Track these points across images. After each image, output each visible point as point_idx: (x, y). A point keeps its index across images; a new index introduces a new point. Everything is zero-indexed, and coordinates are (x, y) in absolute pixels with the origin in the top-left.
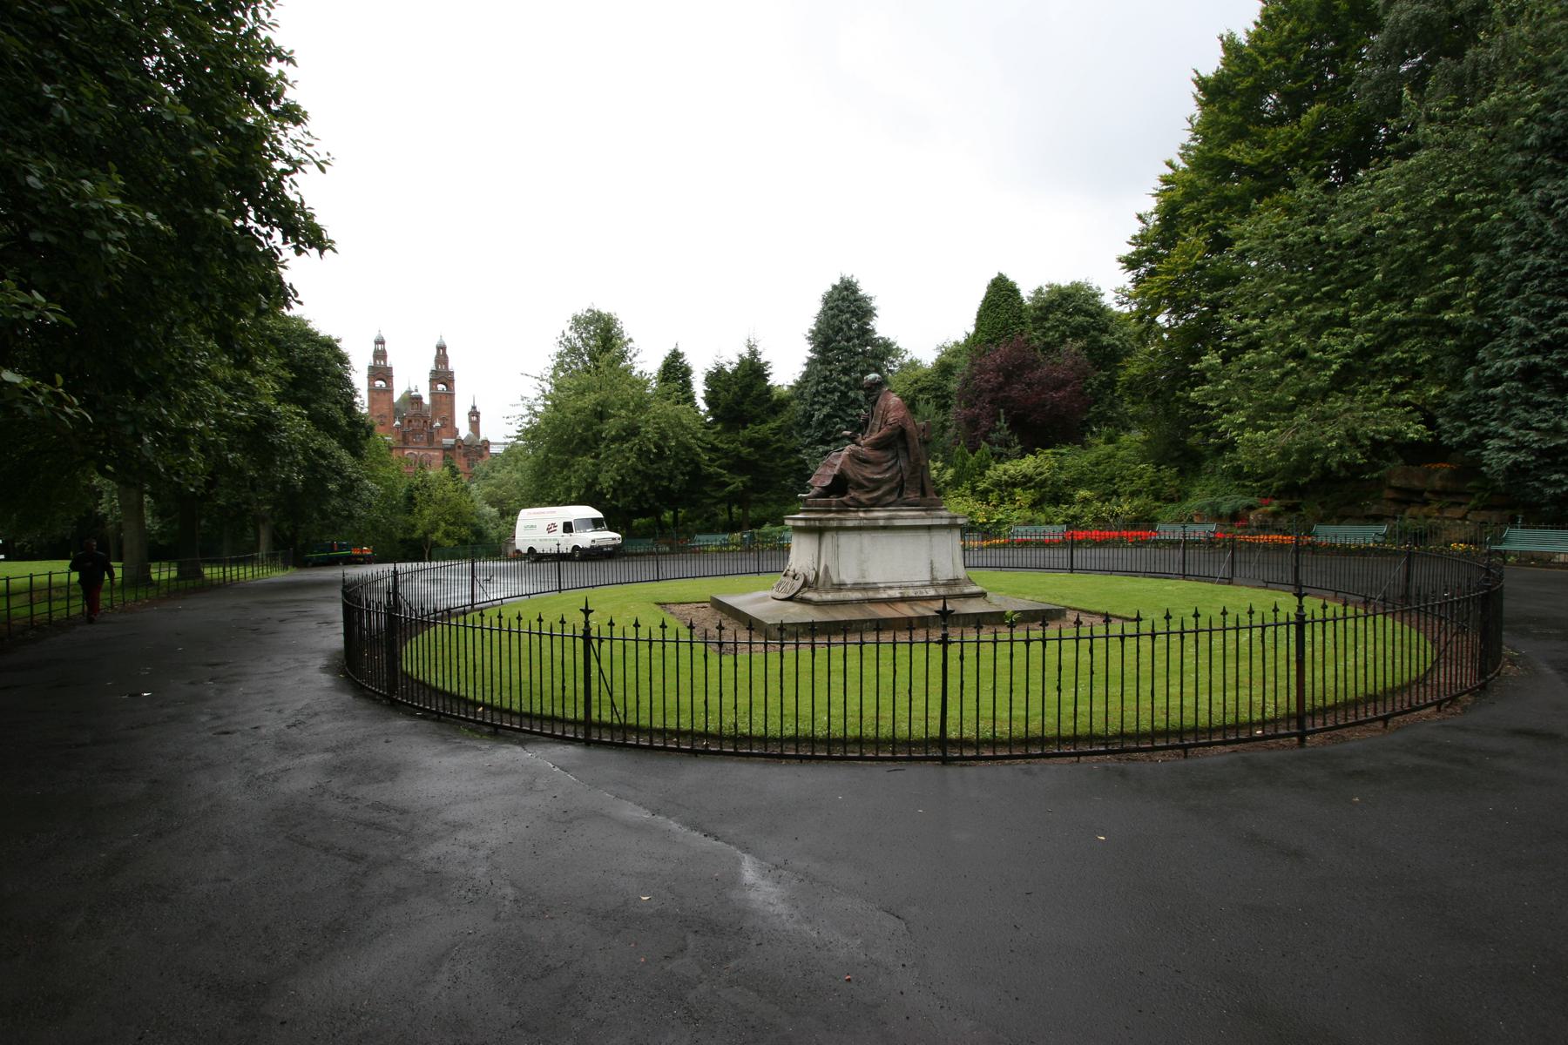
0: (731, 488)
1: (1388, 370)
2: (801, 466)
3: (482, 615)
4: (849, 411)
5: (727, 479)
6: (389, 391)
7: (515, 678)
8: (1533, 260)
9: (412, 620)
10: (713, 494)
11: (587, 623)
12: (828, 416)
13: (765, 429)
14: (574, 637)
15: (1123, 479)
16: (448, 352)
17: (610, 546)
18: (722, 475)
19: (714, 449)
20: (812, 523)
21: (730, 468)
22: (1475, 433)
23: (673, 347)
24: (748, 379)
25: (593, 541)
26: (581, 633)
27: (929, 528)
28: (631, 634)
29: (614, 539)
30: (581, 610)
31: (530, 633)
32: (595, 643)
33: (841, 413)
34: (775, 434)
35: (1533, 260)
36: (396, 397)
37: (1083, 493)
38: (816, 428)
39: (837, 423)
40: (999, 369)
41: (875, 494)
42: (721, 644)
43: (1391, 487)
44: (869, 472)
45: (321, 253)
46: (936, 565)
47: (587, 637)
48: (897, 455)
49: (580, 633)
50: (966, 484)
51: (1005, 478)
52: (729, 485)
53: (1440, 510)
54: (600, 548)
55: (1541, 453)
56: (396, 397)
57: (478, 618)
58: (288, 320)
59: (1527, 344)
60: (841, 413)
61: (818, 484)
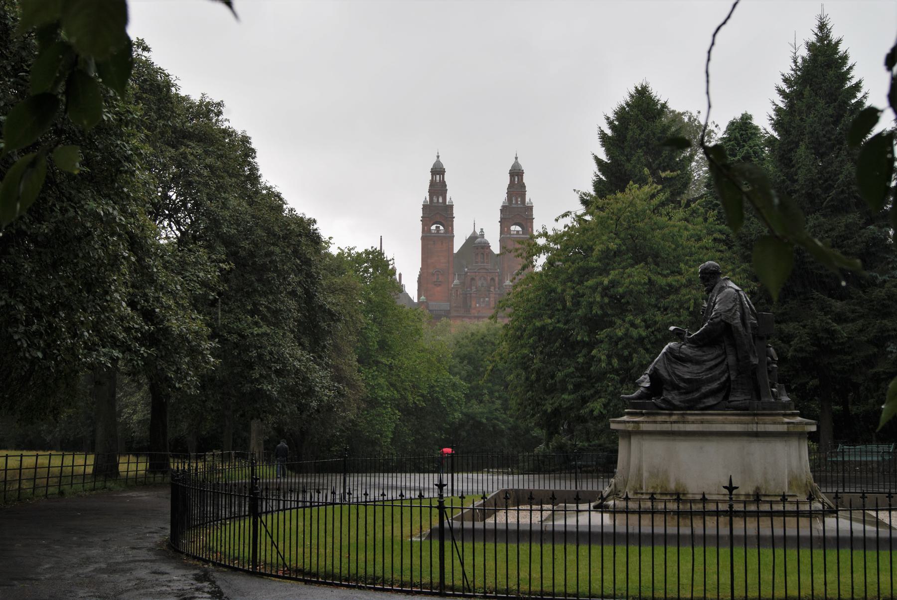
6: (449, 237)
7: (379, 536)
11: (441, 496)
14: (431, 507)
16: (526, 180)
26: (437, 504)
27: (756, 435)
32: (448, 511)
36: (458, 244)
41: (690, 397)
42: (866, 452)
44: (686, 372)
46: (733, 479)
47: (441, 508)
48: (725, 353)
49: (436, 503)
56: (458, 244)
58: (782, 120)
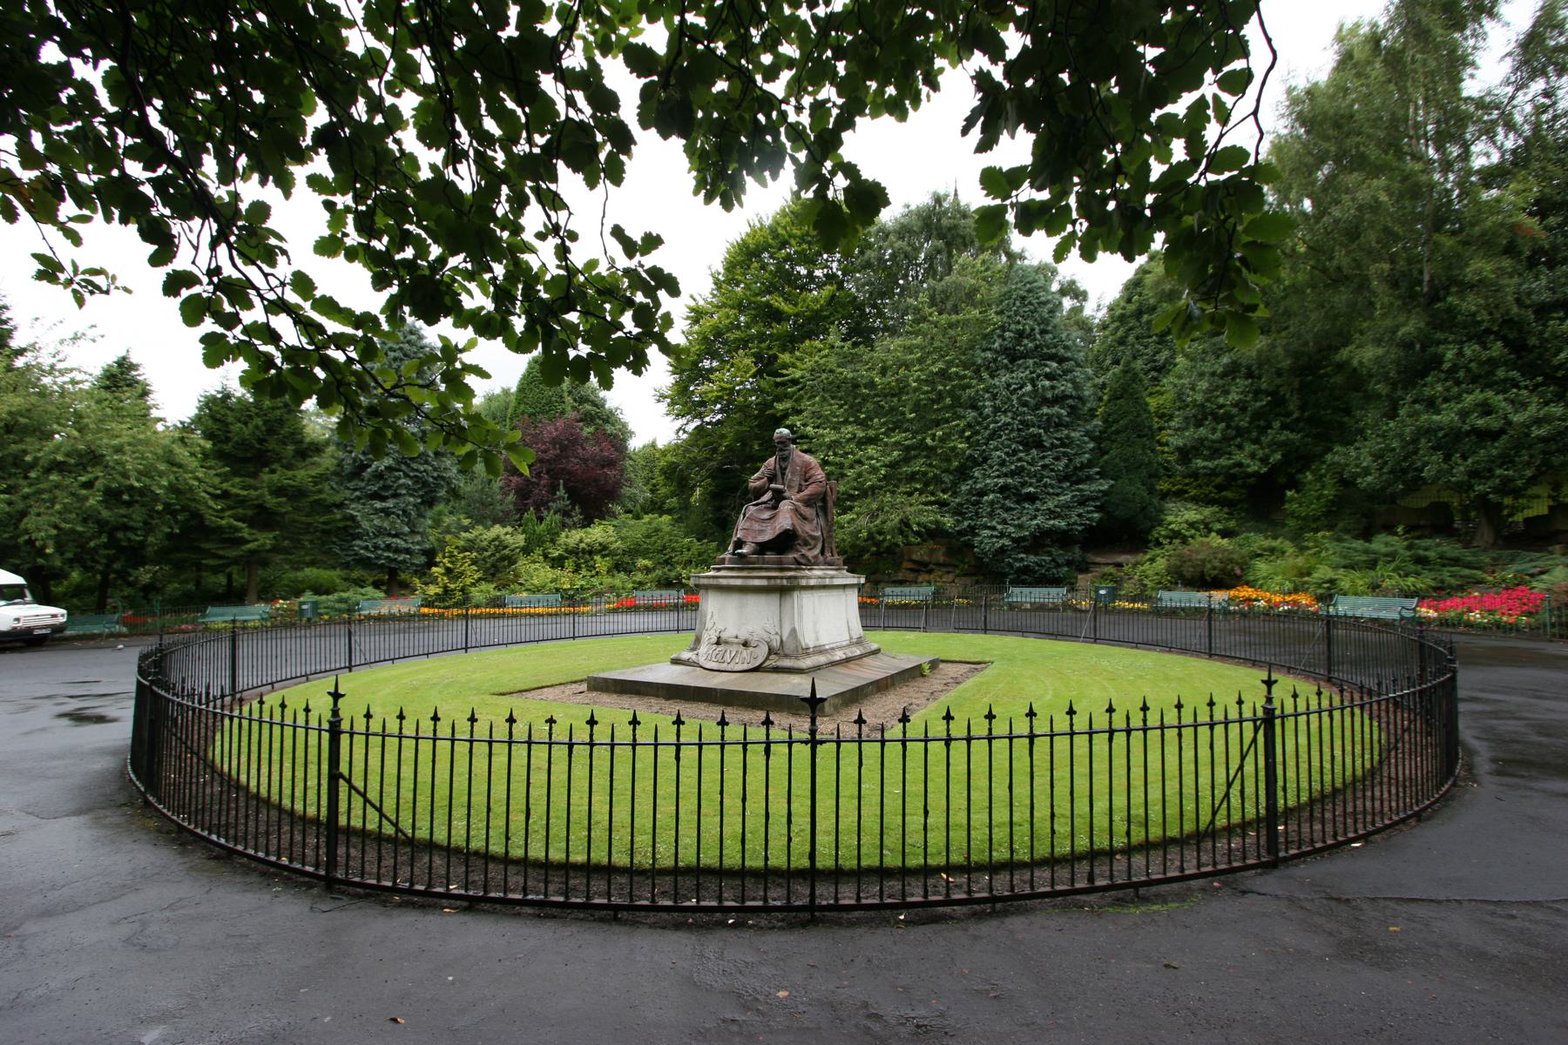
0: (250, 546)
1: (912, 477)
2: (349, 523)
3: (261, 703)
4: (415, 466)
5: (246, 536)
8: (1004, 419)
9: (215, 714)
10: (221, 552)
11: (335, 712)
12: (389, 468)
13: (302, 475)
15: (673, 550)
17: (46, 627)
18: (238, 530)
19: (225, 495)
20: (778, 581)
21: (252, 523)
22: (969, 526)
23: (122, 353)
24: (278, 413)
25: (18, 620)
28: (393, 727)
29: (54, 616)
30: (329, 693)
31: (307, 729)
33: (403, 467)
34: (316, 484)
35: (1004, 419)
37: (642, 562)
38: (369, 480)
39: (399, 478)
40: (554, 441)
43: (911, 560)
45: (689, 307)
47: (335, 731)
50: (539, 551)
51: (582, 545)
52: (248, 542)
53: (941, 577)
54: (29, 630)
55: (1014, 540)
57: (256, 705)
59: (1004, 470)
60: (403, 467)
61: (750, 539)
